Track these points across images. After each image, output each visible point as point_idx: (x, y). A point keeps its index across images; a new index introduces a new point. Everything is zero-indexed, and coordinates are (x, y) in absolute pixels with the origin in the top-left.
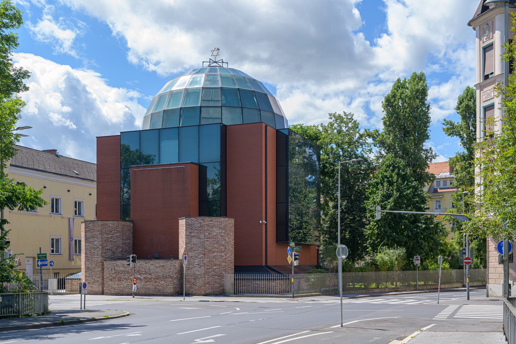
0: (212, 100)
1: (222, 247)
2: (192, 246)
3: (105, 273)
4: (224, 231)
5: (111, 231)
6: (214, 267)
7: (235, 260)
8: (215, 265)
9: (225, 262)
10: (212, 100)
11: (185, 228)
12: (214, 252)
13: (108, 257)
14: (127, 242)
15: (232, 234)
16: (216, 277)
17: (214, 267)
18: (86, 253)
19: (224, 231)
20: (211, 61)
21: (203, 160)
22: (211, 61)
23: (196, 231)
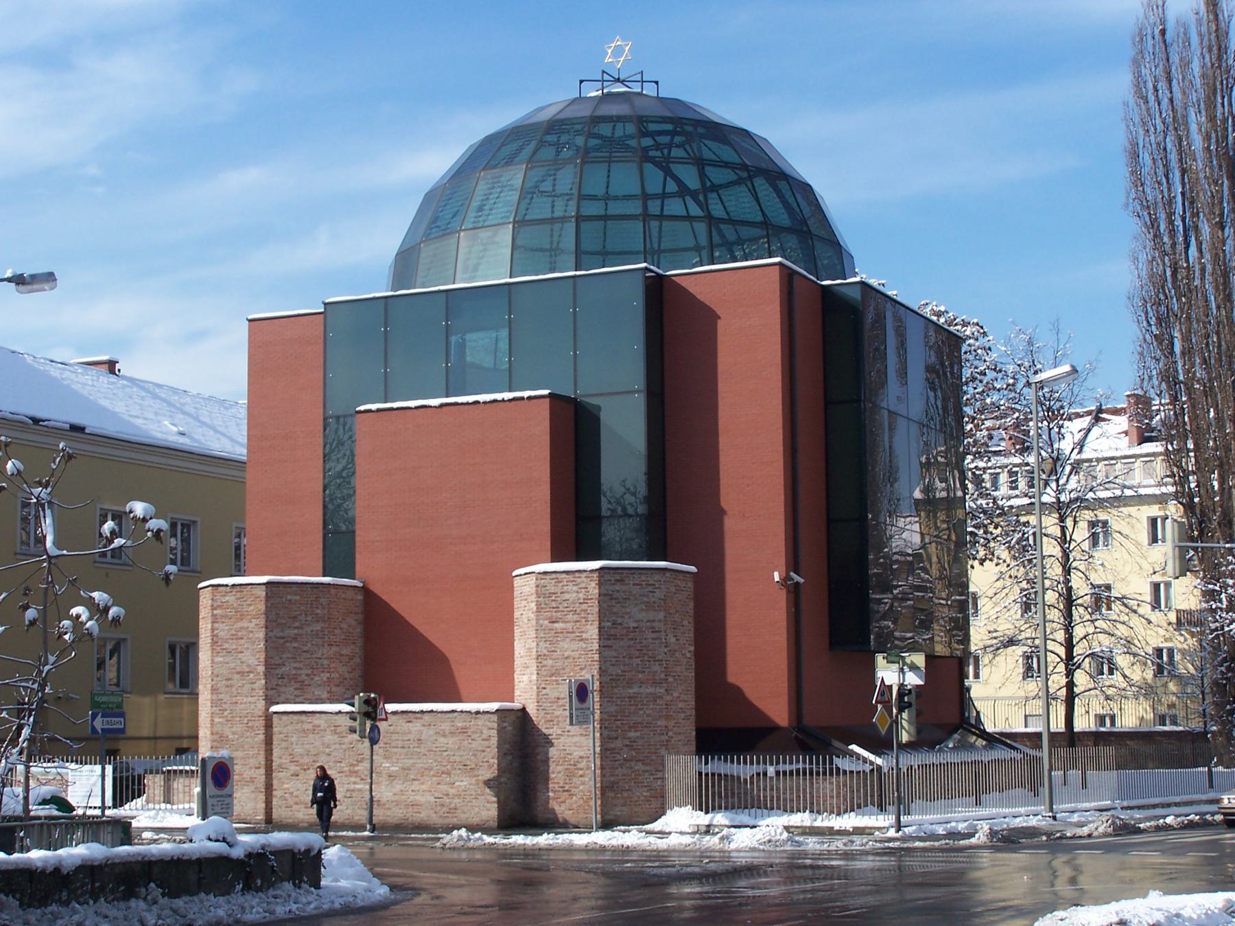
0: (660, 238)
1: (656, 668)
2: (559, 664)
3: (275, 755)
4: (662, 615)
5: (295, 618)
6: (632, 734)
7: (697, 710)
8: (635, 727)
9: (668, 717)
10: (660, 238)
11: (533, 605)
12: (630, 683)
13: (1070, 849)
14: (344, 652)
15: (688, 625)
16: (640, 766)
17: (632, 734)
18: (214, 690)
19: (662, 615)
20: (606, 77)
21: (585, 390)
22: (606, 77)
23: (570, 617)
